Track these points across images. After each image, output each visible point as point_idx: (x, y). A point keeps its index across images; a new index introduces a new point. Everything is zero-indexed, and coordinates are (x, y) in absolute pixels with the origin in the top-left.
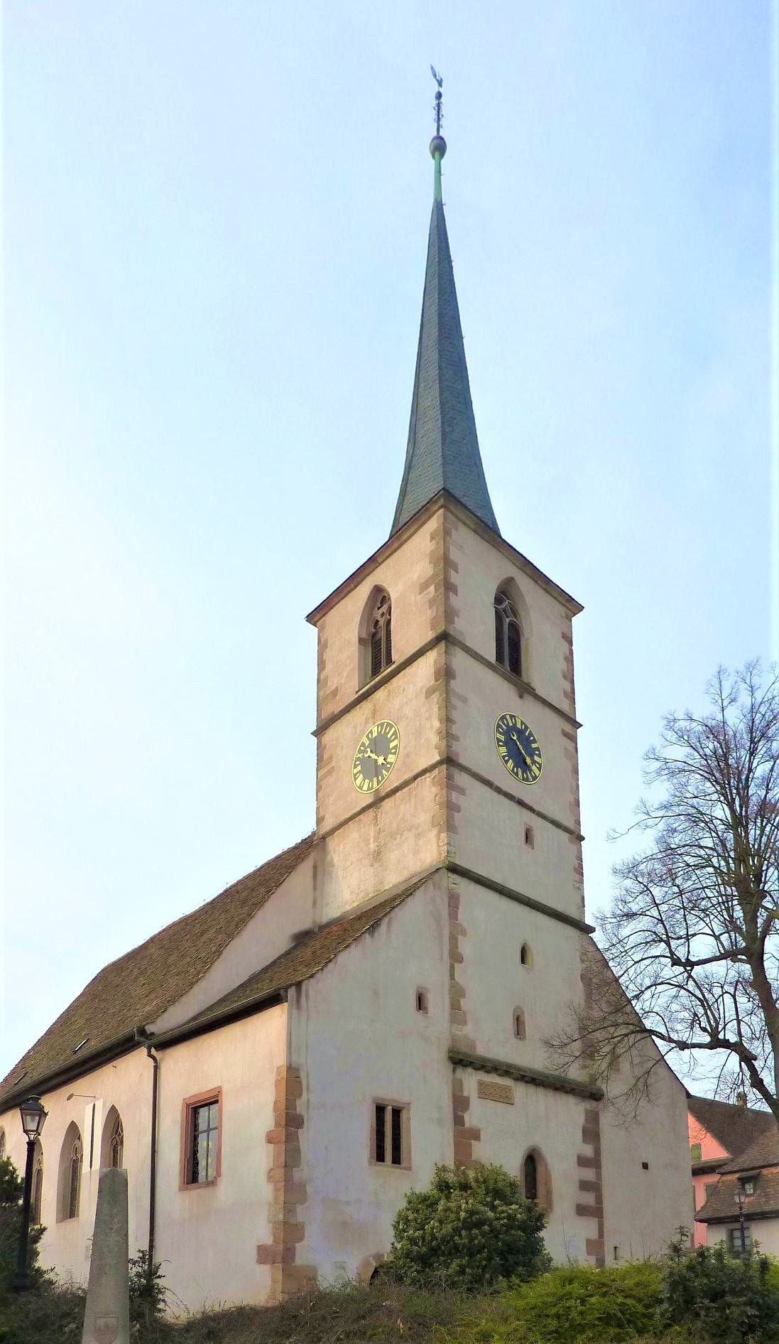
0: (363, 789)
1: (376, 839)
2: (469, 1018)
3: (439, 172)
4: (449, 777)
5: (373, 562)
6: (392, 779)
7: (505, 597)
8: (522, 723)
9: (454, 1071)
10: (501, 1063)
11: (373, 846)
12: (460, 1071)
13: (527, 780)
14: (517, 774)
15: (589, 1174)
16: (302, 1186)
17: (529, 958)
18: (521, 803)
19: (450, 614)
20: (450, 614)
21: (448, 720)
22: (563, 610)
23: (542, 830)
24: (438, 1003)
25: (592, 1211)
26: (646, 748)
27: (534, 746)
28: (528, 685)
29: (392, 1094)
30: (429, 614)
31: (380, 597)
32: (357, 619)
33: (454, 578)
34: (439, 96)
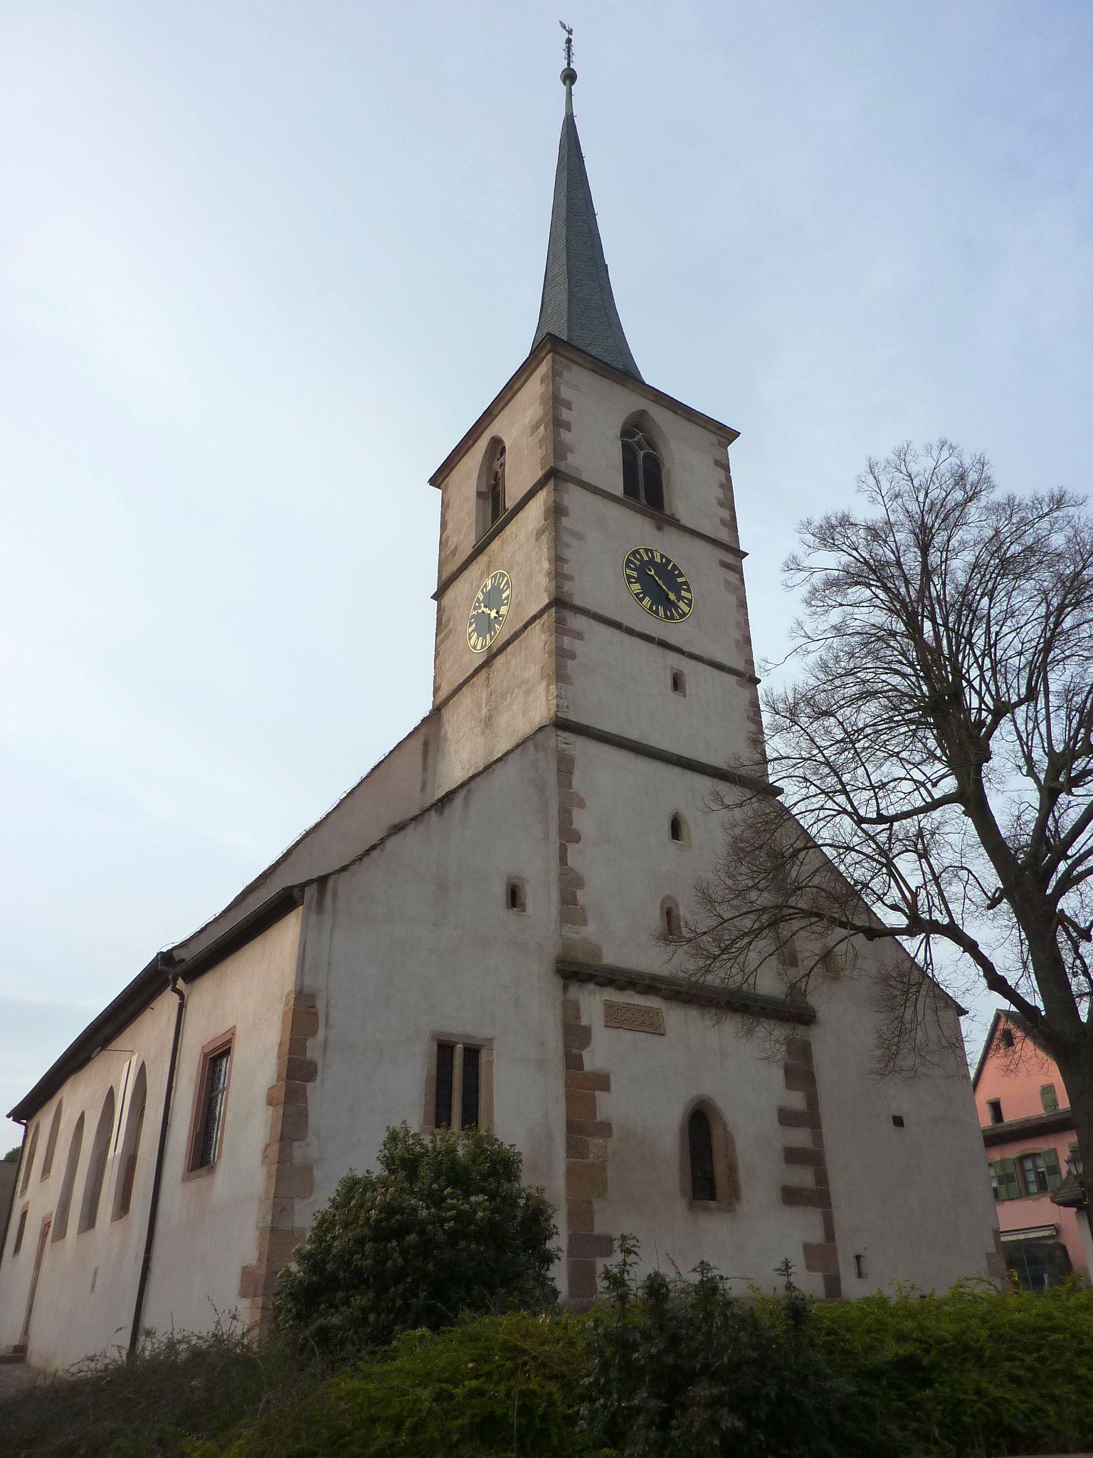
0: (477, 645)
3: (570, 94)
4: (560, 621)
5: (489, 415)
6: (502, 632)
8: (662, 556)
9: (565, 989)
10: (640, 975)
12: (575, 992)
13: (672, 618)
14: (657, 612)
15: (800, 1138)
16: (308, 1169)
18: (663, 644)
19: (560, 450)
20: (560, 450)
21: (558, 559)
22: (714, 438)
23: (695, 674)
24: (542, 900)
25: (812, 1195)
26: (785, 556)
27: (679, 580)
29: (462, 1022)
30: (540, 453)
31: (497, 447)
32: (476, 475)
33: (565, 414)
34: (569, 41)
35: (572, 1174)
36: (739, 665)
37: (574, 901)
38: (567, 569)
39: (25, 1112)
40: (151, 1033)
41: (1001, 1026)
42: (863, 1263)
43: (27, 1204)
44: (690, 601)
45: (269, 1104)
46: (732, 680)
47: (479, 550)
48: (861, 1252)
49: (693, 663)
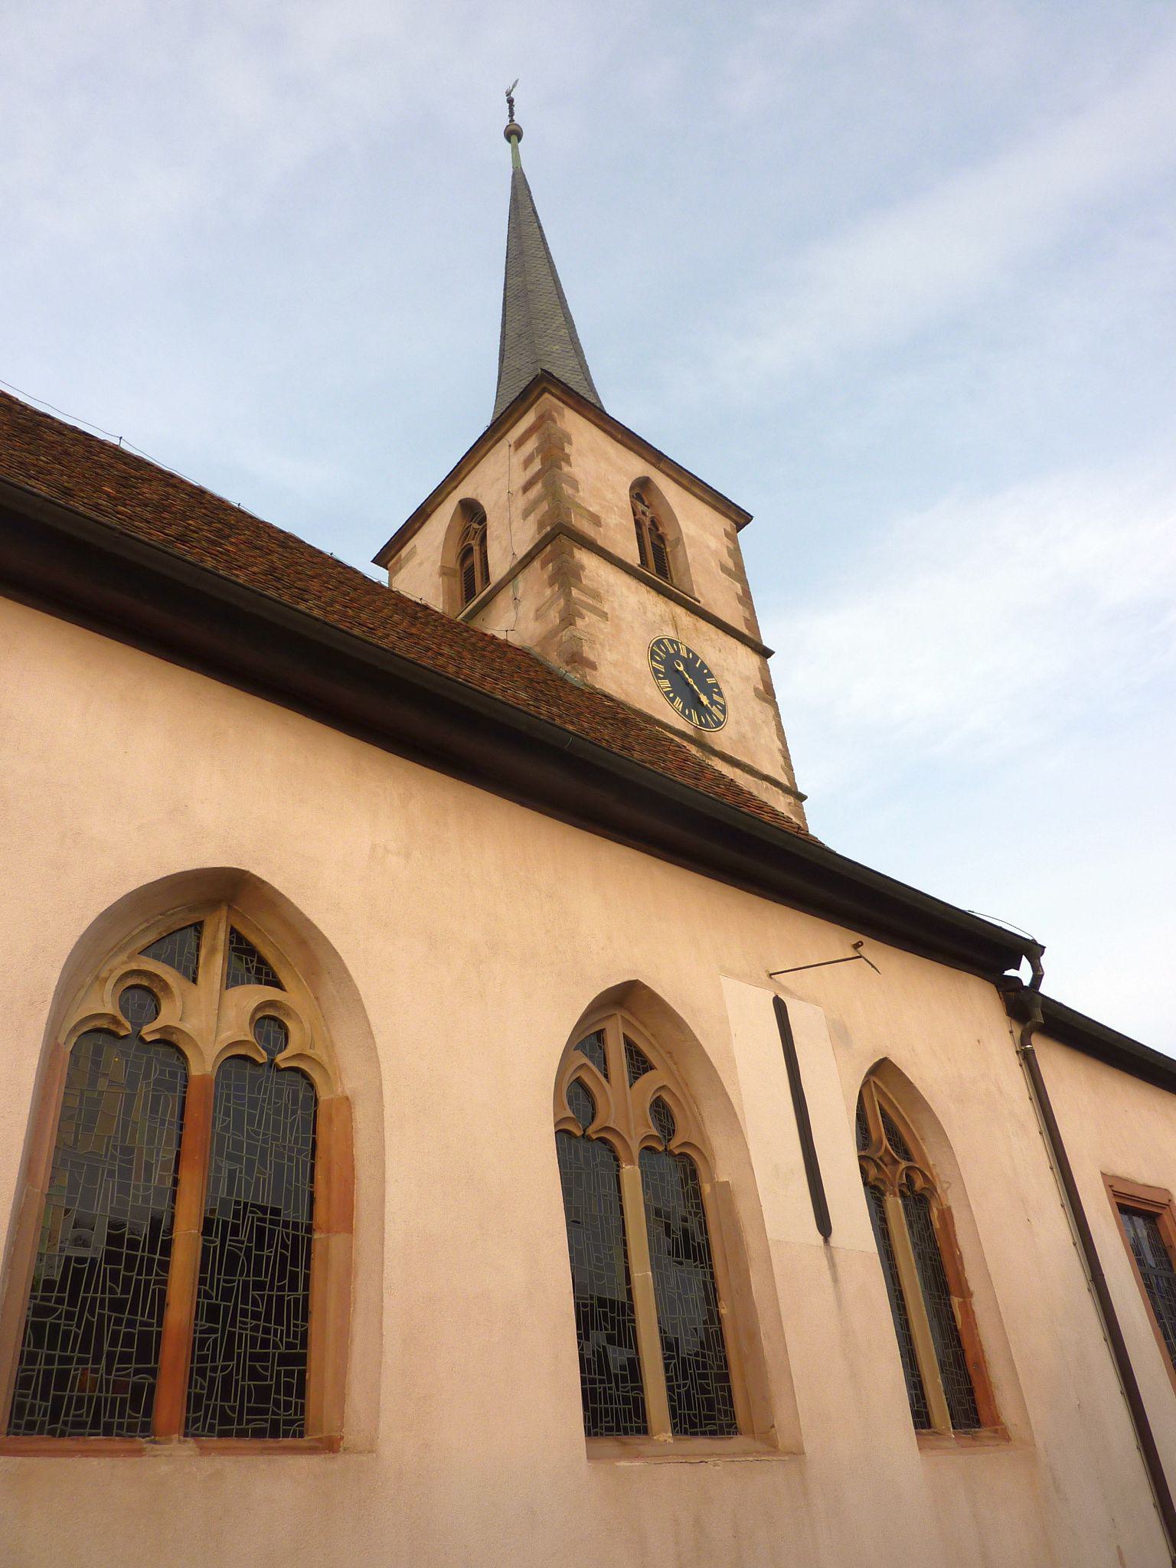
3: (511, 114)
7: (641, 490)
8: (688, 651)
22: (727, 524)
27: (710, 681)
31: (472, 511)
41: (300, 1291)
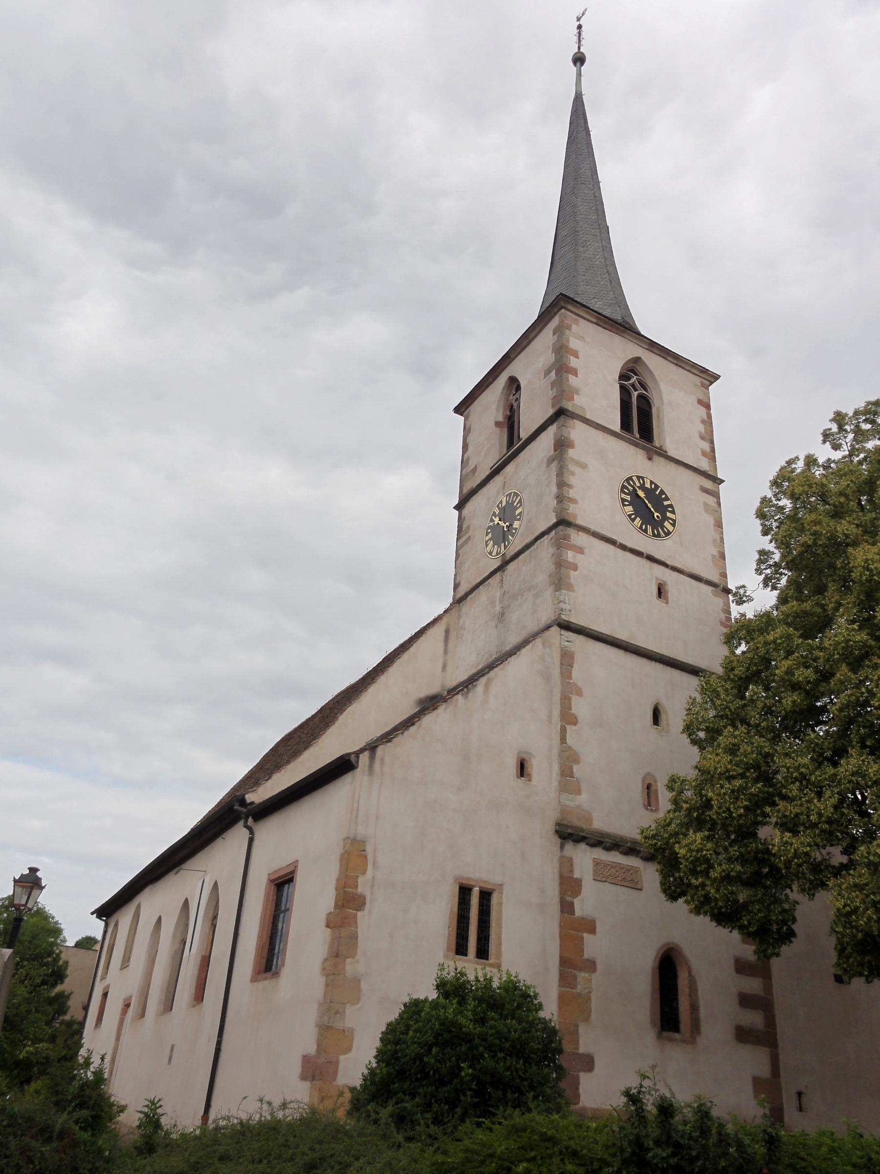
1: (501, 601)
2: (583, 786)
3: (579, 75)
6: (516, 544)
7: (631, 373)
9: (562, 847)
11: (498, 608)
12: (569, 847)
13: (659, 536)
14: (646, 531)
15: (753, 985)
16: (356, 981)
17: (663, 718)
18: (651, 559)
24: (545, 771)
27: (666, 503)
28: (661, 448)
29: (480, 873)
31: (514, 384)
32: (494, 407)
34: (580, 27)
35: (563, 1000)
36: (715, 578)
37: (571, 775)
38: (572, 493)
39: (107, 911)
40: (225, 857)
42: (804, 1099)
43: (108, 986)
44: (674, 521)
45: (327, 926)
46: (708, 589)
47: (496, 471)
48: (803, 1090)
49: (676, 574)
